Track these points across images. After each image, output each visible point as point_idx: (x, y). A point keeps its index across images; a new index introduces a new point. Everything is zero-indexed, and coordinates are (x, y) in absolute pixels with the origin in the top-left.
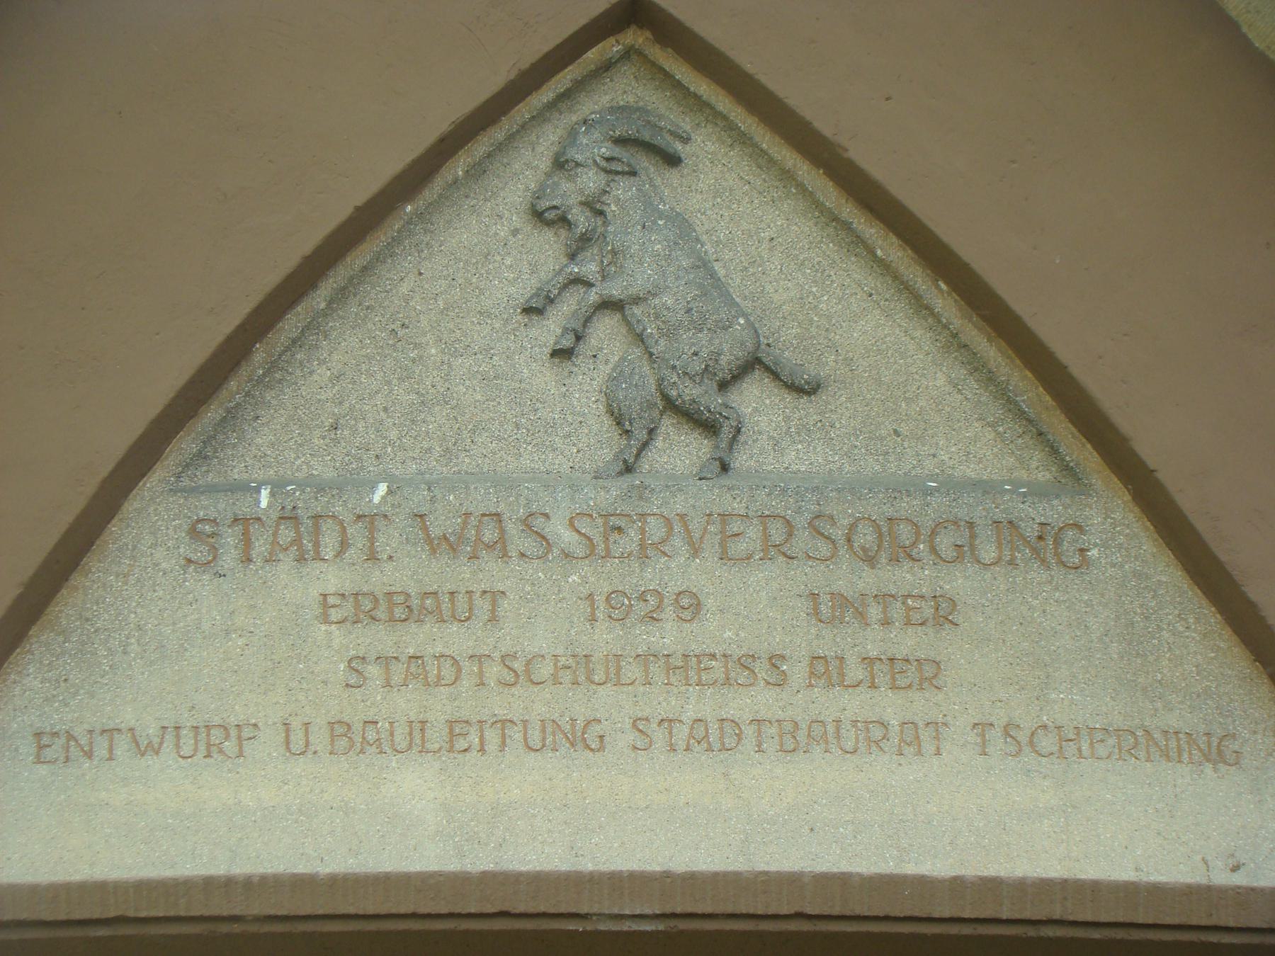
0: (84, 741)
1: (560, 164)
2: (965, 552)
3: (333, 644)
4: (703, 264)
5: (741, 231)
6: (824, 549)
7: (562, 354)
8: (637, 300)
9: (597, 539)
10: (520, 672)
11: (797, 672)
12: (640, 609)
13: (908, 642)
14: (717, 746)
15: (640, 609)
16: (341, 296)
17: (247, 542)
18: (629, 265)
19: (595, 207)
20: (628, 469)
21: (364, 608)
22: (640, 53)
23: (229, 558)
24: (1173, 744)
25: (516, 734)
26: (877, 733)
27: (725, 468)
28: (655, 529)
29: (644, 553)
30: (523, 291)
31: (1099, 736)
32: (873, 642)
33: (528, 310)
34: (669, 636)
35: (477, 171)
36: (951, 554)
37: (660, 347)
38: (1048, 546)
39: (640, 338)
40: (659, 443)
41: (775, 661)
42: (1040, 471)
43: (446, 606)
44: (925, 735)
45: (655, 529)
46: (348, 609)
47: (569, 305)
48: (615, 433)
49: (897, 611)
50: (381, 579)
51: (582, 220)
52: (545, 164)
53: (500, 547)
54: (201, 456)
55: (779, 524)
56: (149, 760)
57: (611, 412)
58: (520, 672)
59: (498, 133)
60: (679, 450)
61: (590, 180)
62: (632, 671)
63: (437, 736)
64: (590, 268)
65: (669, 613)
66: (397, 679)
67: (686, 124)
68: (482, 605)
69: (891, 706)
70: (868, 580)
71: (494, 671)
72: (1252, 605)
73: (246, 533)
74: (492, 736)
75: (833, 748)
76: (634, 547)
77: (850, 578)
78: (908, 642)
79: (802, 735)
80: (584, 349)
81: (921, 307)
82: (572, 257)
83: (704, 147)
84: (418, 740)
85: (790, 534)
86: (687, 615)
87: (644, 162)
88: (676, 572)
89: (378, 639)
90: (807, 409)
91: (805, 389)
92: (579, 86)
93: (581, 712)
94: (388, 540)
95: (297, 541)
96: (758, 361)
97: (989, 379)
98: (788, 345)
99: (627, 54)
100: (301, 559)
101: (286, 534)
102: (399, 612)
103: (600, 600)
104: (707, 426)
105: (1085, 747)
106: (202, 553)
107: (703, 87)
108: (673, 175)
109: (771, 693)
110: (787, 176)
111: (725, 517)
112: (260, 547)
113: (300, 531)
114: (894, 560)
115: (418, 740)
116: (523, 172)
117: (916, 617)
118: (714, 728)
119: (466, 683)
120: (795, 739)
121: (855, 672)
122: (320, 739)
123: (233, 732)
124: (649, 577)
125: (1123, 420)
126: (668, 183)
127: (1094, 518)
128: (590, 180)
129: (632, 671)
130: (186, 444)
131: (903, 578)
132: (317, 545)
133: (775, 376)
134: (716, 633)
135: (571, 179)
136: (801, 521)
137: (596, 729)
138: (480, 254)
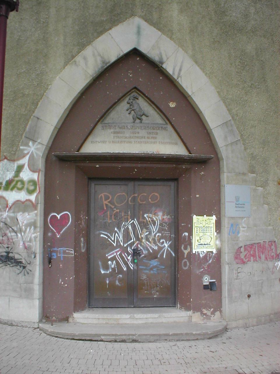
1: (129, 99)
2: (159, 129)
3: (112, 135)
4: (140, 107)
5: (143, 104)
7: (129, 114)
12: (135, 133)
16: (113, 109)
17: (106, 127)
19: (132, 103)
20: (134, 122)
21: (115, 133)
23: (105, 129)
25: (125, 142)
27: (141, 122)
28: (136, 127)
29: (135, 129)
30: (127, 109)
32: (152, 136)
33: (28, 274)
34: (137, 135)
35: (123, 100)
39: (135, 113)
40: (136, 120)
42: (164, 123)
45: (136, 127)
47: (130, 110)
50: (116, 130)
51: (131, 104)
52: (128, 99)
53: (125, 128)
54: (103, 121)
56: (99, 143)
58: (126, 138)
59: (125, 97)
60: (138, 121)
61: (132, 100)
64: (131, 107)
65: (137, 133)
68: (123, 133)
69: (153, 140)
71: (124, 137)
74: (124, 142)
77: (150, 131)
78: (154, 136)
81: (156, 110)
82: (130, 106)
83: (140, 98)
87: (136, 99)
88: (137, 130)
89: (116, 135)
91: (147, 116)
92: (131, 93)
94: (116, 128)
97: (161, 116)
98: (146, 113)
101: (109, 127)
104: (140, 119)
106: (103, 128)
107: (140, 93)
108: (138, 100)
109: (144, 139)
110: (146, 101)
111: (141, 126)
112: (107, 128)
116: (127, 100)
120: (146, 143)
121: (150, 138)
122: (111, 142)
126: (137, 101)
128: (132, 100)
130: (101, 120)
131: (154, 131)
133: (145, 116)
134: (140, 135)
136: (147, 127)
138: (124, 105)
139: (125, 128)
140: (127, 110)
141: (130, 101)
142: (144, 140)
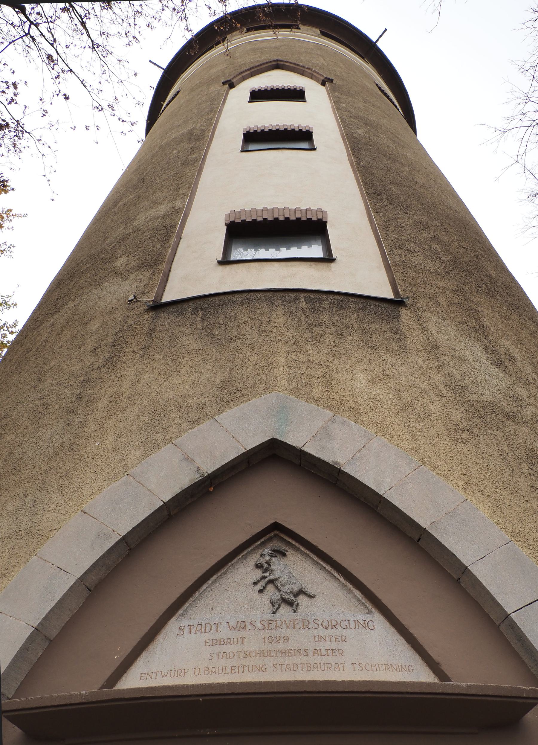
0: (150, 675)
6: (316, 626)
7: (261, 591)
8: (276, 579)
9: (266, 626)
10: (247, 655)
11: (311, 653)
12: (275, 640)
13: (335, 646)
14: (292, 670)
15: (275, 640)
18: (275, 573)
19: (268, 563)
21: (216, 642)
22: (278, 535)
24: (397, 667)
25: (246, 668)
26: (329, 666)
28: (279, 623)
30: (254, 580)
31: (380, 666)
34: (282, 646)
35: (245, 557)
36: (345, 627)
37: (281, 589)
38: (366, 625)
40: (281, 608)
41: (306, 651)
43: (232, 641)
44: (341, 666)
45: (279, 623)
46: (211, 643)
47: (263, 583)
48: (272, 607)
49: (333, 639)
50: (218, 636)
51: (265, 566)
53: (245, 628)
55: (306, 621)
57: (271, 602)
60: (285, 610)
61: (267, 558)
62: (273, 654)
63: (228, 670)
65: (282, 641)
66: (220, 657)
67: (287, 549)
70: (326, 633)
72: (411, 634)
73: (191, 628)
74: (241, 670)
75: (319, 669)
76: (274, 627)
79: (312, 667)
80: (266, 590)
83: (290, 553)
84: (224, 671)
85: (309, 624)
86: (286, 641)
88: (283, 632)
89: (218, 649)
90: (313, 600)
91: (312, 597)
93: (261, 663)
94: (221, 628)
95: (201, 629)
96: (302, 591)
98: (309, 590)
99: (276, 536)
100: (202, 633)
101: (199, 627)
102: (222, 643)
103: (266, 639)
105: (378, 668)
112: (193, 631)
113: (202, 628)
114: (332, 628)
115: (224, 671)
116: (254, 558)
117: (337, 640)
118: (292, 666)
119: (236, 657)
123: (183, 671)
124: (278, 633)
125: (380, 595)
127: (376, 623)
128: (267, 558)
129: (273, 654)
131: (333, 632)
132: (205, 629)
134: (292, 645)
135: (263, 558)
137: (264, 667)
138: (244, 573)
139: (245, 628)
140: (255, 584)
141: (262, 561)
142: (302, 659)
